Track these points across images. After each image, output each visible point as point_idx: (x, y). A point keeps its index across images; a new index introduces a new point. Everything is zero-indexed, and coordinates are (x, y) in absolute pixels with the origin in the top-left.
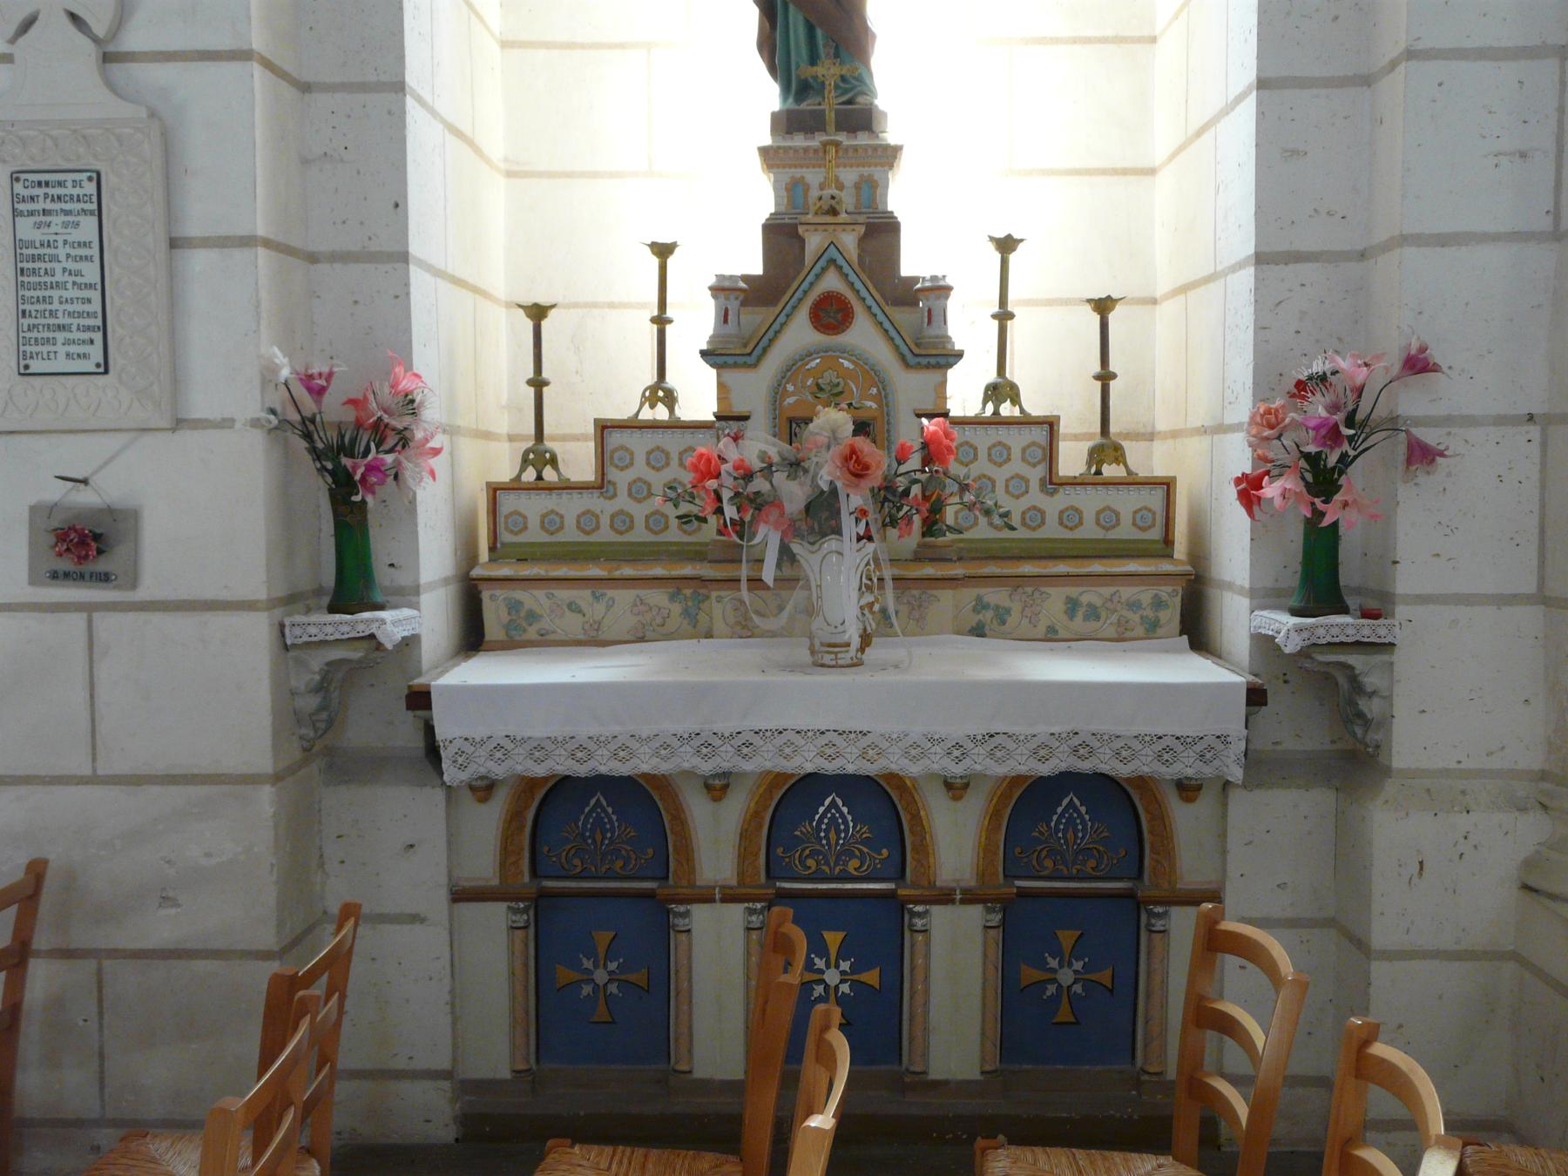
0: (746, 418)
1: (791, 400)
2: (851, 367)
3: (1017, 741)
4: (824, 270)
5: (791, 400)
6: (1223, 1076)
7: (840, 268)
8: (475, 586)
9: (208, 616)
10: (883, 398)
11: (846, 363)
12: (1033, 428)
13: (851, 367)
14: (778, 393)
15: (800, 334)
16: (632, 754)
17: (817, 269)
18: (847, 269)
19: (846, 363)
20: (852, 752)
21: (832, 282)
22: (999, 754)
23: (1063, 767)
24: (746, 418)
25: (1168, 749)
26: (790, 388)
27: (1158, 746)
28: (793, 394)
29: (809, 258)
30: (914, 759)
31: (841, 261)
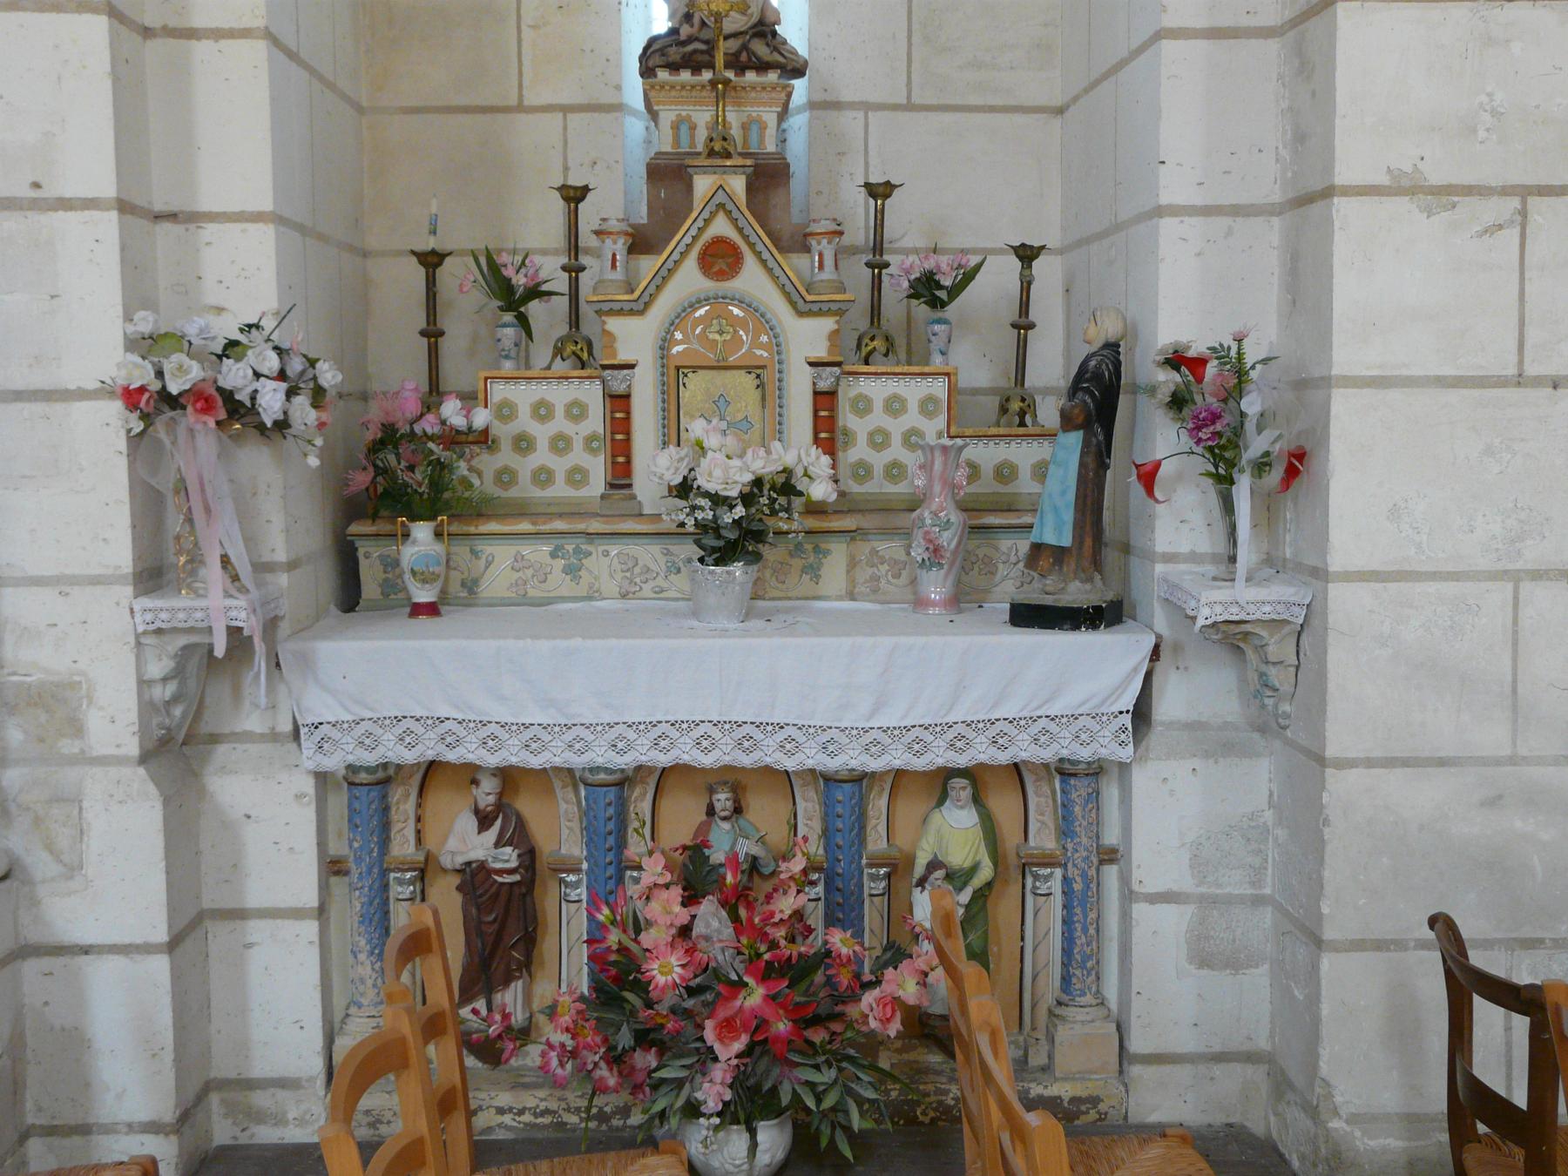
0: (631, 366)
1: (679, 348)
2: (742, 314)
3: (977, 730)
4: (713, 215)
5: (679, 348)
6: (795, 1051)
7: (728, 213)
8: (352, 543)
9: (1517, 274)
10: (777, 347)
11: (736, 311)
12: (48, 570)
13: (742, 314)
14: (665, 345)
15: (689, 279)
16: (1053, 739)
17: (706, 214)
18: (736, 214)
19: (736, 311)
20: (645, 742)
21: (721, 227)
22: (663, 743)
23: (727, 760)
24: (631, 366)
25: (876, 742)
26: (678, 336)
27: (950, 735)
28: (679, 343)
29: (698, 203)
30: (918, 754)
31: (730, 206)
